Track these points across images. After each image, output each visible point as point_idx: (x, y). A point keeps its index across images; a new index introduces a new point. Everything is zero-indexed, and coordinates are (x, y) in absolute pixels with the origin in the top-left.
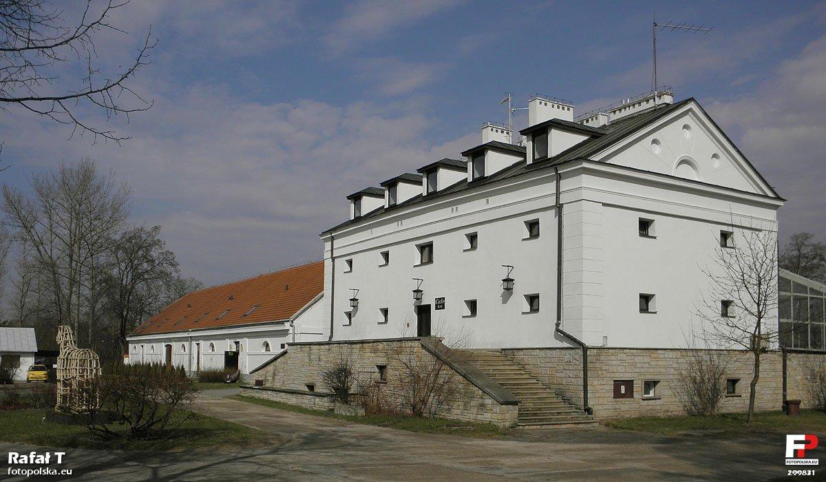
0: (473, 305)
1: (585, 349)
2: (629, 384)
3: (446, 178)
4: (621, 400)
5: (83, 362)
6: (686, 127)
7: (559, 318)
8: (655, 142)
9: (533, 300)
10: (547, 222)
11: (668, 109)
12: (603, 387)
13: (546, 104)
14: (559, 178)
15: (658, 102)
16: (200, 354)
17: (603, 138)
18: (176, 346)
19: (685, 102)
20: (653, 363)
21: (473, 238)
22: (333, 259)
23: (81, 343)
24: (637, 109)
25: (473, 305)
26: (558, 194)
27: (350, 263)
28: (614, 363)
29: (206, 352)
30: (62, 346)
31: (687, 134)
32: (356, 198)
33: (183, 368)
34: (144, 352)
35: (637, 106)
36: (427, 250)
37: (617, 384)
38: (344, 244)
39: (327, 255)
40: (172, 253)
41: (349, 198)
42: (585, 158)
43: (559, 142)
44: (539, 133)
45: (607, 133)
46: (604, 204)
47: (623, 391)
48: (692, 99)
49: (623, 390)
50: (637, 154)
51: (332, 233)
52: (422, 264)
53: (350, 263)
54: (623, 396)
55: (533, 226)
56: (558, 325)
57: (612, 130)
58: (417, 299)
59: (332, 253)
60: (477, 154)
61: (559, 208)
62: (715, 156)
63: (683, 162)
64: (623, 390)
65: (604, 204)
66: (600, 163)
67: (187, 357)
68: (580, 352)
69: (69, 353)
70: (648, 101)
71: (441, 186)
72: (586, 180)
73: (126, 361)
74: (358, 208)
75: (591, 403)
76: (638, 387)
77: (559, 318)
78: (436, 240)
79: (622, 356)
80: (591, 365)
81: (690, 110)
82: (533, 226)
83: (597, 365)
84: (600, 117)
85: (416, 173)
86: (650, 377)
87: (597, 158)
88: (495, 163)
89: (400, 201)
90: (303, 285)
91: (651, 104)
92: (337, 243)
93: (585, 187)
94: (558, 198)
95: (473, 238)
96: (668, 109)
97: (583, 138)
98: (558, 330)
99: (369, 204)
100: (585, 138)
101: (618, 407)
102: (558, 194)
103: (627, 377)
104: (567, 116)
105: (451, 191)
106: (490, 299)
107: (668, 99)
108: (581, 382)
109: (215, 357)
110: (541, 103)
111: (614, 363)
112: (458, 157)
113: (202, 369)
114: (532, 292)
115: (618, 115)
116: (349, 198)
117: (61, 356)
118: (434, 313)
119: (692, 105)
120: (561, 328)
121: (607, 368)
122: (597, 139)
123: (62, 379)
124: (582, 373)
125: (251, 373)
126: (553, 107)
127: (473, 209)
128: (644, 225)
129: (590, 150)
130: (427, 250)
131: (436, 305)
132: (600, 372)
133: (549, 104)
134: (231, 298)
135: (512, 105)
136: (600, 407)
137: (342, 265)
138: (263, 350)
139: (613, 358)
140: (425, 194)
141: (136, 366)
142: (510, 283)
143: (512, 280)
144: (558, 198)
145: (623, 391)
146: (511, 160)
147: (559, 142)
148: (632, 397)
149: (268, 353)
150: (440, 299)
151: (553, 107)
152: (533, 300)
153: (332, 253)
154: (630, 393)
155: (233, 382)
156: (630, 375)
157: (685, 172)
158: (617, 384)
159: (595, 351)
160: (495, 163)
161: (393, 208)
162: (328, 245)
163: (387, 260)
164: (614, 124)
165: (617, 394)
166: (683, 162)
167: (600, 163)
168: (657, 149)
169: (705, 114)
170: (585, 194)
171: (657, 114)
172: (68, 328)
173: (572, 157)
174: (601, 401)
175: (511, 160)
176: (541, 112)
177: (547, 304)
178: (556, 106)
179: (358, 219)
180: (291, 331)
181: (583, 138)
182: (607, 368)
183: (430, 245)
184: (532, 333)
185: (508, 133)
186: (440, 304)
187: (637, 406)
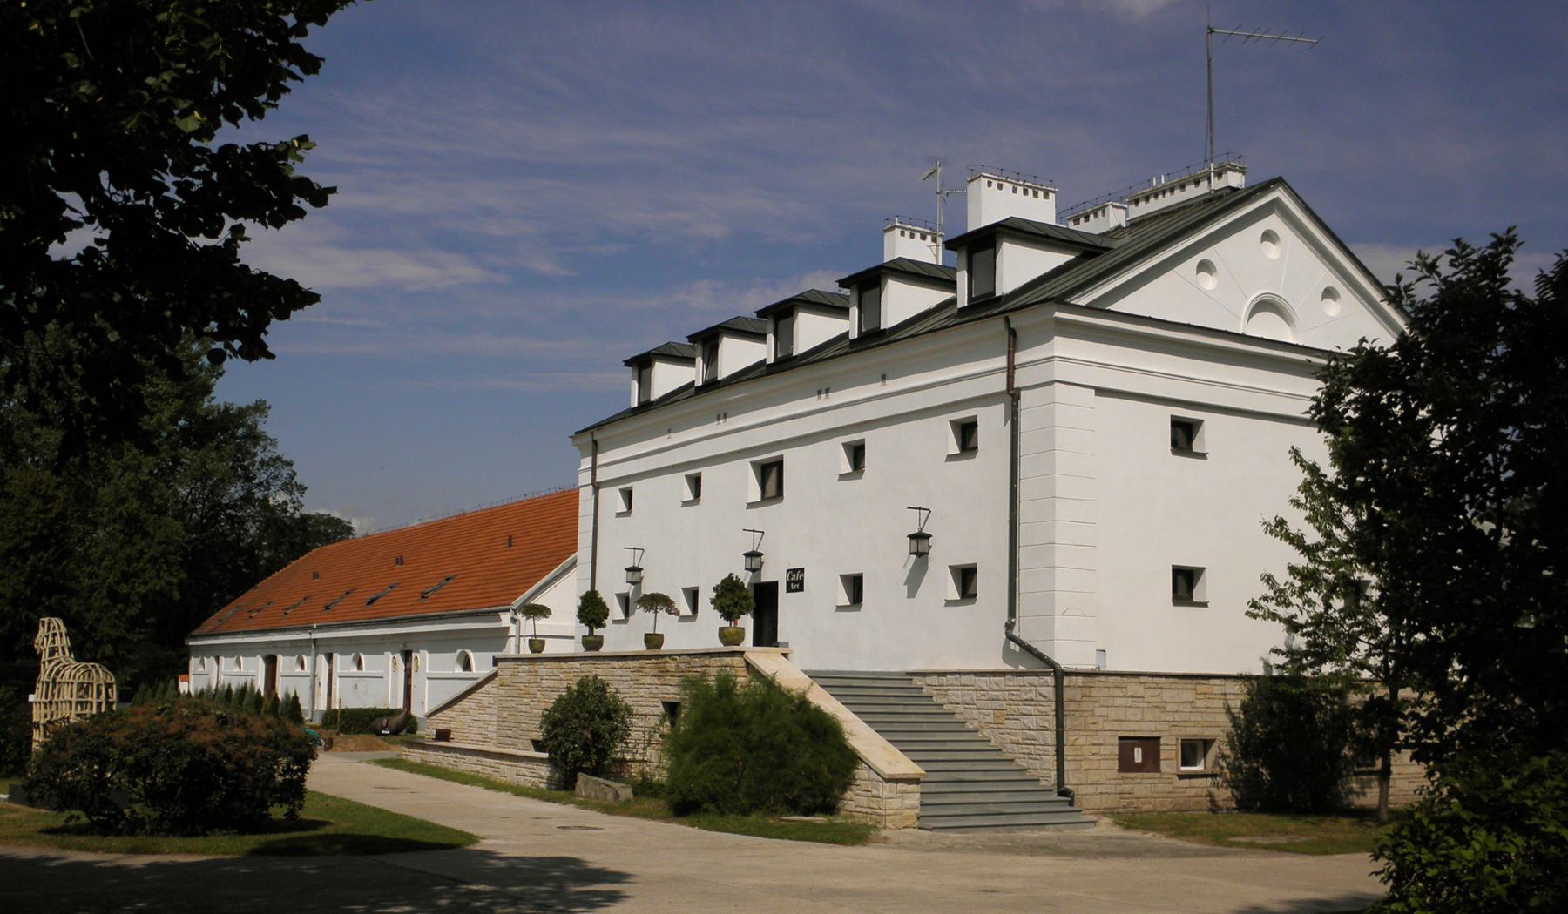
0: (855, 585)
1: (1060, 674)
2: (1151, 745)
3: (811, 330)
4: (1133, 775)
5: (84, 688)
6: (1269, 236)
7: (1012, 612)
8: (1205, 267)
9: (966, 577)
10: (992, 423)
11: (1229, 200)
12: (1095, 749)
13: (1000, 187)
14: (1014, 341)
15: (1217, 184)
16: (324, 681)
17: (1107, 255)
18: (284, 663)
19: (1265, 187)
20: (1199, 703)
21: (857, 454)
22: (597, 487)
23: (81, 651)
24: (1179, 197)
25: (855, 585)
26: (1011, 369)
27: (628, 495)
28: (1119, 701)
29: (346, 672)
30: (45, 657)
31: (1272, 251)
32: (642, 364)
33: (296, 698)
34: (216, 671)
35: (1177, 191)
36: (771, 474)
37: (1127, 743)
38: (616, 460)
39: (585, 478)
40: (290, 464)
41: (628, 363)
42: (1061, 301)
43: (1018, 266)
44: (978, 246)
45: (1116, 244)
46: (1101, 392)
47: (1138, 758)
48: (1279, 181)
49: (1138, 755)
50: (1170, 295)
51: (593, 438)
52: (766, 499)
53: (628, 495)
54: (1139, 768)
55: (966, 433)
56: (1010, 626)
57: (1127, 239)
58: (753, 570)
59: (594, 475)
60: (868, 283)
61: (1012, 396)
62: (1329, 293)
63: (1265, 305)
64: (1138, 755)
65: (1101, 392)
66: (1090, 309)
67: (307, 682)
68: (1050, 680)
69: (58, 672)
70: (1197, 183)
71: (801, 345)
72: (1061, 346)
73: (183, 687)
74: (644, 384)
75: (1071, 780)
76: (1170, 752)
77: (1012, 612)
78: (790, 457)
79: (1134, 688)
80: (1073, 706)
81: (1276, 202)
82: (966, 433)
83: (1085, 706)
84: (1111, 210)
85: (686, 341)
86: (1193, 732)
87: (1083, 300)
88: (902, 302)
89: (724, 371)
90: (540, 535)
91: (1203, 189)
92: (602, 459)
93: (1067, 357)
94: (1010, 379)
95: (857, 454)
96: (1229, 200)
97: (1059, 259)
98: (1010, 638)
99: (667, 378)
100: (1069, 257)
101: (1127, 788)
102: (1011, 369)
103: (1146, 730)
104: (1042, 210)
105: (817, 355)
106: (885, 568)
107: (1235, 180)
108: (1051, 737)
109: (362, 683)
110: (989, 184)
111: (1119, 701)
112: (833, 288)
113: (336, 706)
114: (964, 560)
115: (1144, 209)
116: (628, 363)
117: (43, 677)
118: (785, 600)
119: (1279, 193)
120: (1015, 633)
121: (1104, 711)
122: (1092, 257)
123: (43, 721)
124: (1053, 721)
125: (429, 716)
126: (1015, 191)
127: (856, 399)
128: (1184, 435)
129: (1073, 283)
130: (771, 474)
131: (789, 584)
132: (1090, 720)
133: (1008, 187)
134: (400, 561)
135: (942, 185)
136: (1091, 789)
137: (612, 499)
138: (459, 670)
139: (1117, 692)
140: (771, 360)
141: (201, 694)
142: (923, 543)
143: (928, 537)
144: (1010, 379)
145: (1138, 758)
146: (930, 297)
147: (1018, 266)
148: (1157, 769)
149: (467, 674)
150: (795, 571)
151: (1015, 191)
152: (966, 577)
153: (594, 475)
154: (1153, 761)
155: (395, 732)
156: (1152, 726)
157: (1267, 327)
158: (1127, 743)
159: (1080, 679)
160: (902, 302)
161: (712, 385)
162: (587, 463)
163: (697, 493)
164: (1135, 224)
165: (1126, 764)
166: (1265, 305)
167: (1090, 309)
168: (1209, 282)
169: (1307, 209)
170: (1060, 371)
171: (1218, 206)
172: (58, 624)
173: (1044, 294)
174: (1093, 777)
175: (930, 297)
176: (992, 203)
177: (991, 584)
178: (1020, 189)
179: (646, 406)
180: (513, 631)
181: (1059, 259)
182: (1104, 711)
183: (779, 464)
184: (956, 642)
185: (934, 240)
186: (796, 582)
187: (1168, 788)
